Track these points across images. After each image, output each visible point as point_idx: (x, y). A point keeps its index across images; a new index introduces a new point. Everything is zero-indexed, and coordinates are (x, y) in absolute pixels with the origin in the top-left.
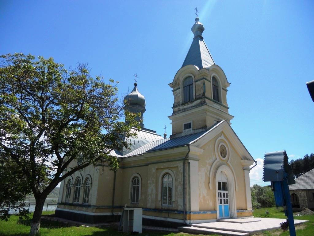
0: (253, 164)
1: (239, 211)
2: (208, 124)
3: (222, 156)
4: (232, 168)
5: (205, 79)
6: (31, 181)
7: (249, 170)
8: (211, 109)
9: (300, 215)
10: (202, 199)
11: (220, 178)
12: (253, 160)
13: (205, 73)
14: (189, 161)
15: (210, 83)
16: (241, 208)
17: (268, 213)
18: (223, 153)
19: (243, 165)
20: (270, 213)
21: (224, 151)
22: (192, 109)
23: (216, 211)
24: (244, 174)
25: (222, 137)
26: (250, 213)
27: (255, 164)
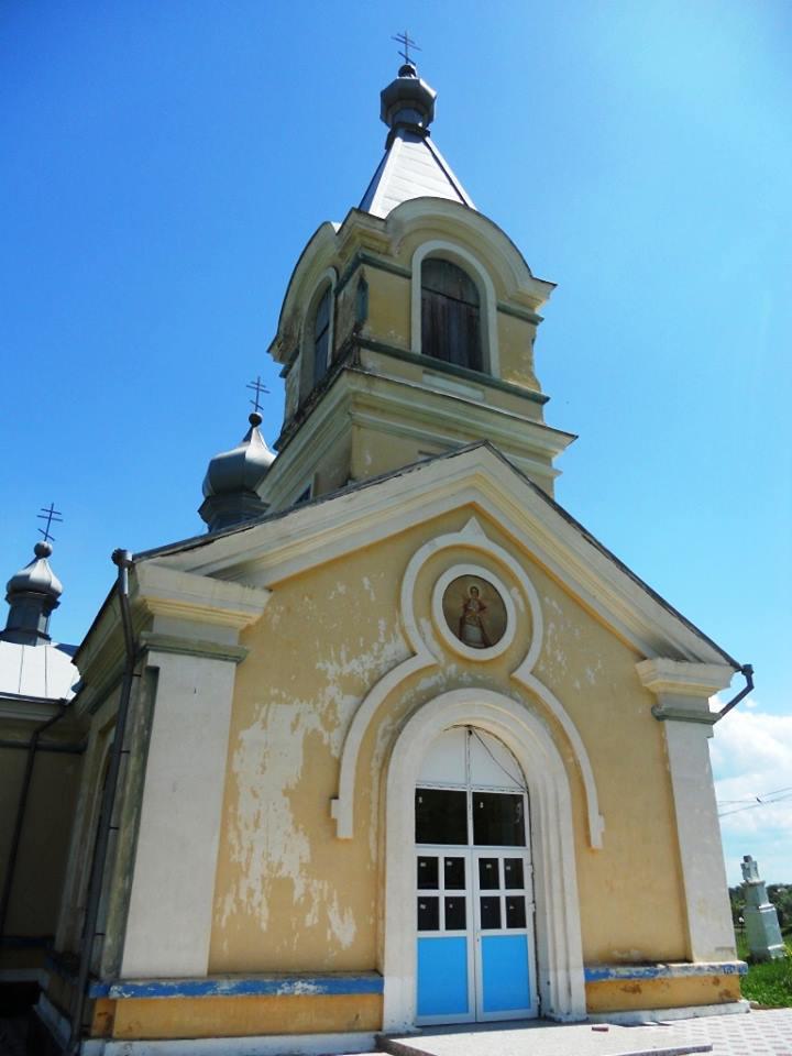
0: (728, 686)
1: (606, 975)
2: (365, 461)
3: (468, 643)
5: (367, 260)
7: (711, 719)
8: (382, 393)
10: (258, 897)
11: (438, 757)
13: (362, 234)
14: (153, 659)
15: (404, 281)
16: (635, 954)
18: (475, 616)
19: (653, 695)
22: (302, 426)
23: (382, 976)
24: (663, 742)
25: (472, 535)
26: (717, 981)
27: (745, 685)
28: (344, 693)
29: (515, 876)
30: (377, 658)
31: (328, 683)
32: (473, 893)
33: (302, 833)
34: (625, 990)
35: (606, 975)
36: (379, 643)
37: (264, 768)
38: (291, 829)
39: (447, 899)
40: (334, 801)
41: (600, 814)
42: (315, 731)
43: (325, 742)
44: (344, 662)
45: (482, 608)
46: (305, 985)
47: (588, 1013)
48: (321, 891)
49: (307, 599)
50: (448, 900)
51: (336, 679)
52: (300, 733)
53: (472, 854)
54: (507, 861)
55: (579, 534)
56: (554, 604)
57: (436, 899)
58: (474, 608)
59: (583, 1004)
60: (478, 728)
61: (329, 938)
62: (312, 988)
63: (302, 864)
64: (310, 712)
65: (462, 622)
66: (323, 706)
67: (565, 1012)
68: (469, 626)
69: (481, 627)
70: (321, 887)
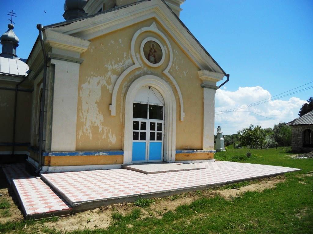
1: (181, 152)
3: (151, 62)
4: (174, 82)
6: (152, 108)
7: (216, 88)
9: (305, 158)
12: (221, 72)
14: (53, 61)
16: (189, 147)
17: (249, 155)
18: (153, 54)
19: (202, 81)
20: (253, 155)
21: (155, 51)
23: (123, 151)
24: (203, 93)
25: (153, 28)
26: (208, 154)
27: (227, 79)
29: (160, 127)
32: (148, 131)
38: (98, 112)
39: (141, 132)
40: (110, 106)
43: (108, 88)
46: (103, 153)
50: (141, 133)
52: (100, 86)
54: (158, 123)
57: (138, 132)
58: (153, 51)
61: (109, 141)
62: (105, 154)
64: (103, 80)
69: (155, 57)
70: (106, 128)
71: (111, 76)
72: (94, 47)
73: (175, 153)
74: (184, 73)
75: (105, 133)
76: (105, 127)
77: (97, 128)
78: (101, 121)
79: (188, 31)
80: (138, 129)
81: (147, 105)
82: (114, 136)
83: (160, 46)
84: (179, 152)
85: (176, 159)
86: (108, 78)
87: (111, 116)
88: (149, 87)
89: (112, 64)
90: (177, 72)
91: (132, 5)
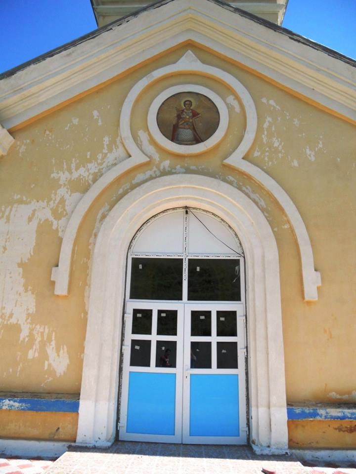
1: (315, 414)
4: (269, 183)
18: (188, 121)
28: (72, 192)
29: (228, 323)
30: (101, 164)
31: (60, 186)
32: (184, 338)
33: (30, 293)
34: (340, 429)
35: (315, 414)
36: (103, 153)
37: (5, 248)
38: (22, 289)
39: (158, 342)
40: (54, 269)
41: (316, 270)
42: (47, 220)
43: (54, 227)
44: (73, 171)
45: (195, 114)
46: (12, 403)
47: (290, 447)
48: (42, 333)
49: (47, 132)
50: (159, 343)
51: (66, 183)
52: (34, 225)
53: (184, 309)
54: (219, 314)
55: (285, 38)
56: (272, 102)
57: (148, 343)
58: (187, 116)
59: (285, 439)
60: (194, 208)
61: (46, 368)
62: (17, 404)
63: (29, 315)
64: (44, 208)
65: (176, 128)
66: (54, 203)
67: (265, 444)
68: (182, 130)
69: (194, 129)
70: (42, 330)
71: (67, 196)
72: (28, 141)
73: (286, 418)
74: (308, 152)
75: (37, 342)
76: (38, 327)
77: (17, 328)
78: (28, 310)
79: (295, 37)
80: (219, 334)
81: (180, 261)
82: (64, 352)
83: (210, 100)
84: (303, 412)
85: (290, 440)
86: (57, 202)
87: (53, 294)
88: (184, 210)
89: (70, 171)
90: (280, 155)
91: (111, 29)
